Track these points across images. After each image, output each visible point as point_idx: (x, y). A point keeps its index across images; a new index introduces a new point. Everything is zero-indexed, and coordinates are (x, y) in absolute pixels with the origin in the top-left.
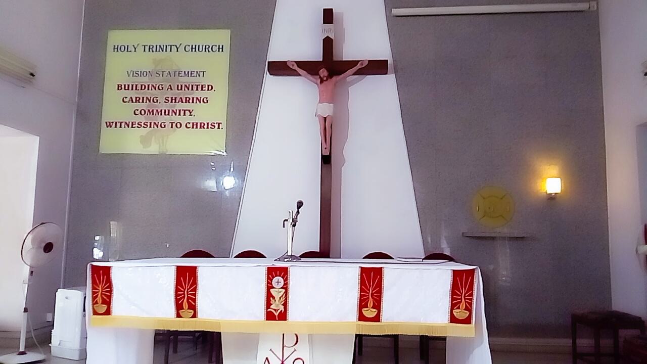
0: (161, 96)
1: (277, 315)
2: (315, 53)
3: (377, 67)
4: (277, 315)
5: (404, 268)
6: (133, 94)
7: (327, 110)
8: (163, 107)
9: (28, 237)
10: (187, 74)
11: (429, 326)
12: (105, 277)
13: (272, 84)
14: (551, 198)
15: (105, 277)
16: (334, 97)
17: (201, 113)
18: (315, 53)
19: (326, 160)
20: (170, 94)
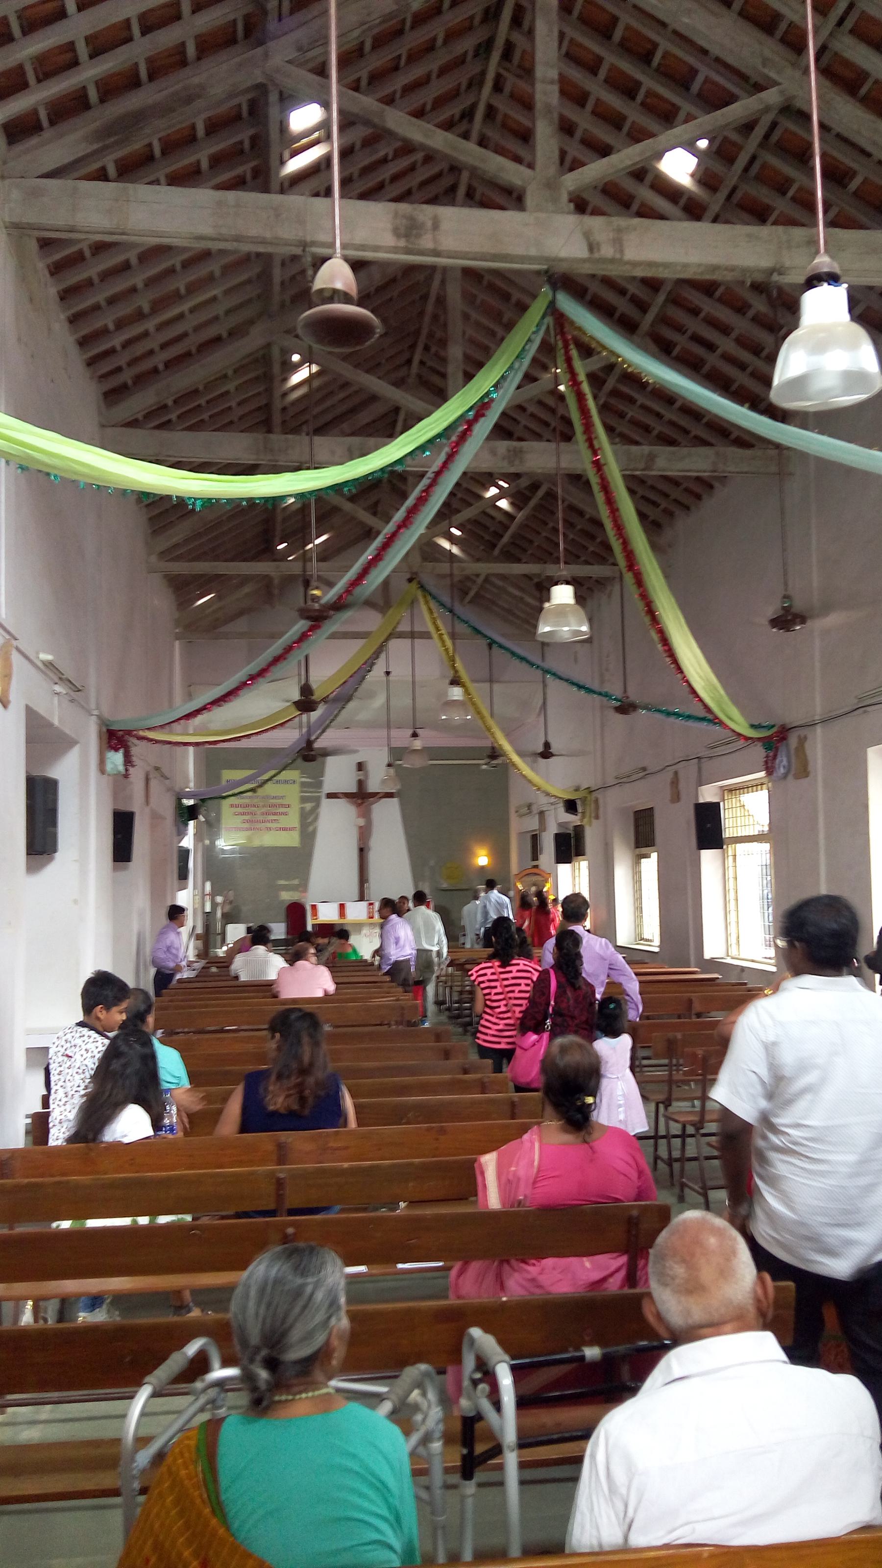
0: (259, 811)
1: (342, 907)
2: (353, 789)
3: (558, 462)
4: (342, 907)
5: (116, 237)
6: (239, 810)
7: (361, 822)
8: (261, 818)
9: (847, 709)
10: (274, 798)
11: (43, 53)
12: (282, 882)
13: (326, 804)
14: (483, 867)
15: (282, 882)
16: (366, 815)
17: (284, 821)
18: (353, 789)
19: (361, 850)
20: (264, 810)
